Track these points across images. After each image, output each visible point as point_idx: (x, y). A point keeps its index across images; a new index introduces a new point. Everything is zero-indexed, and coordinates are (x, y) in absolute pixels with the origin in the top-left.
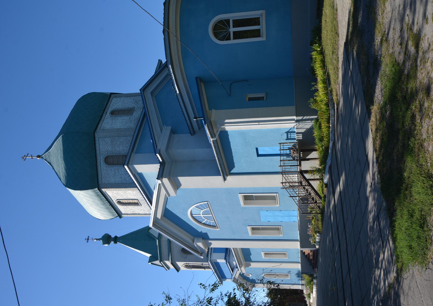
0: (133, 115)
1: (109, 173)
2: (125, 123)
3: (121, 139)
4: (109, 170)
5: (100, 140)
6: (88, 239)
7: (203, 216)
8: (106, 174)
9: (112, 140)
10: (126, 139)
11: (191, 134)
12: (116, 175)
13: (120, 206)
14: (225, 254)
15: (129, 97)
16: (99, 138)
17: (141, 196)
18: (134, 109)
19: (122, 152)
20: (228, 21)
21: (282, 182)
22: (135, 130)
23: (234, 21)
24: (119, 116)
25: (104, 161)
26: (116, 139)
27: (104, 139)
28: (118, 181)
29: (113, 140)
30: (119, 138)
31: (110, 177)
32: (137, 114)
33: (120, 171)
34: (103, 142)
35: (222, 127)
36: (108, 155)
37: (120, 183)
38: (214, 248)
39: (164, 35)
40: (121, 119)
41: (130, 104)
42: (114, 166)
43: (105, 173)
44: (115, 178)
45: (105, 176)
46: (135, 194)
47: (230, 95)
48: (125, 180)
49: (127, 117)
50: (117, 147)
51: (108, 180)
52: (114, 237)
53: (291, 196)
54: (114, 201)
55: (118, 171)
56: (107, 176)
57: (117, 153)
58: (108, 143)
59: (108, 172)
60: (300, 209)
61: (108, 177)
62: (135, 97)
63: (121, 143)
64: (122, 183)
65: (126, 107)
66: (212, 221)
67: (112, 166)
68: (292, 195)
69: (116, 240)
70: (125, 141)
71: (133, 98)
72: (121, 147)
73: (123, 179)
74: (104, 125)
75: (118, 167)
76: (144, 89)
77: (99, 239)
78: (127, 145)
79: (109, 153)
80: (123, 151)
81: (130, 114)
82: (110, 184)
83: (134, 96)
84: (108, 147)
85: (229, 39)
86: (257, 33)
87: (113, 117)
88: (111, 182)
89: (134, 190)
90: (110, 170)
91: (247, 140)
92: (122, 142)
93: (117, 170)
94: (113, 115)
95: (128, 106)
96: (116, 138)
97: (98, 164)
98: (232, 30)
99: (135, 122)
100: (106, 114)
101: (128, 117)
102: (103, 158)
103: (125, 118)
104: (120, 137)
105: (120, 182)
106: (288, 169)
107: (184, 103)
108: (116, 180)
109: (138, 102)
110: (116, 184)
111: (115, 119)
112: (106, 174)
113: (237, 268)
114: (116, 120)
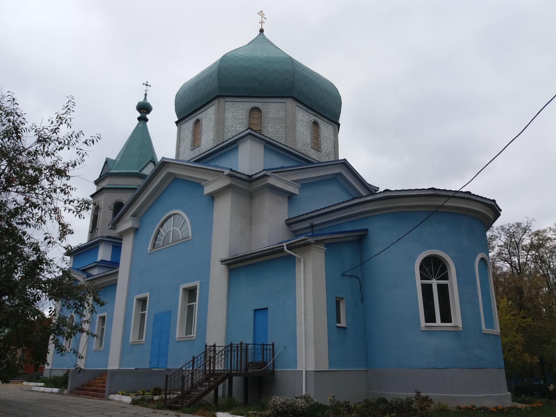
0: (311, 149)
1: (238, 112)
2: (302, 138)
3: (283, 131)
4: (243, 112)
5: (282, 103)
6: (147, 85)
7: (170, 231)
8: (238, 107)
9: (282, 118)
10: (281, 137)
11: (287, 220)
12: (236, 121)
13: (193, 123)
14: (110, 261)
15: (334, 146)
16: (285, 103)
17: (204, 150)
18: (319, 150)
19: (266, 131)
20: (446, 277)
21: (216, 345)
22: (294, 149)
23: (446, 286)
24: (311, 131)
25: (255, 106)
26: (282, 125)
27: (284, 109)
28: (227, 122)
29: (281, 120)
30: (283, 128)
31: (233, 112)
32: (313, 154)
33: (241, 125)
34: (280, 107)
35: (74, 325)
36: (262, 112)
37: (224, 124)
38: (121, 244)
39: (429, 189)
40: (308, 133)
41: (325, 146)
42: (248, 119)
43: (238, 106)
44: (231, 119)
45: (235, 106)
46: (208, 142)
47: (343, 275)
48: (227, 131)
49: (309, 141)
50: (272, 124)
51: (230, 110)
52: (147, 118)
53: (194, 358)
54: (200, 115)
55: (241, 124)
56: (235, 109)
57: (264, 124)
58: (278, 114)
59: (241, 110)
60: (175, 372)
61: (234, 110)
62: (334, 154)
63: (277, 130)
64: (224, 127)
65: (322, 140)
66: (162, 243)
67: (248, 116)
68: (196, 360)
69: (143, 119)
70: (279, 136)
71: (332, 151)
72: (272, 129)
73: (230, 128)
74: (302, 111)
75: (246, 124)
76: (345, 164)
77: (145, 98)
78: (274, 137)
79: (265, 114)
80: (266, 132)
81: (313, 145)
82: (225, 112)
83: (335, 153)
84: (273, 114)
85: (423, 277)
86: (430, 317)
87: (311, 125)
88: (227, 113)
89: (214, 142)
90: (242, 113)
91: (279, 296)
92: (278, 131)
93: (242, 122)
94: (313, 124)
95: (323, 144)
96: (284, 125)
97: (252, 99)
98: (434, 283)
99: (303, 150)
100: (314, 115)
101: (309, 143)
102: (259, 106)
103: (309, 138)
104: (285, 129)
105: (226, 125)
106: (235, 354)
107: (345, 208)
108: (228, 120)
109: (327, 156)
110: (223, 118)
111: (308, 126)
112: (238, 108)
113: (88, 277)
114: (306, 127)
